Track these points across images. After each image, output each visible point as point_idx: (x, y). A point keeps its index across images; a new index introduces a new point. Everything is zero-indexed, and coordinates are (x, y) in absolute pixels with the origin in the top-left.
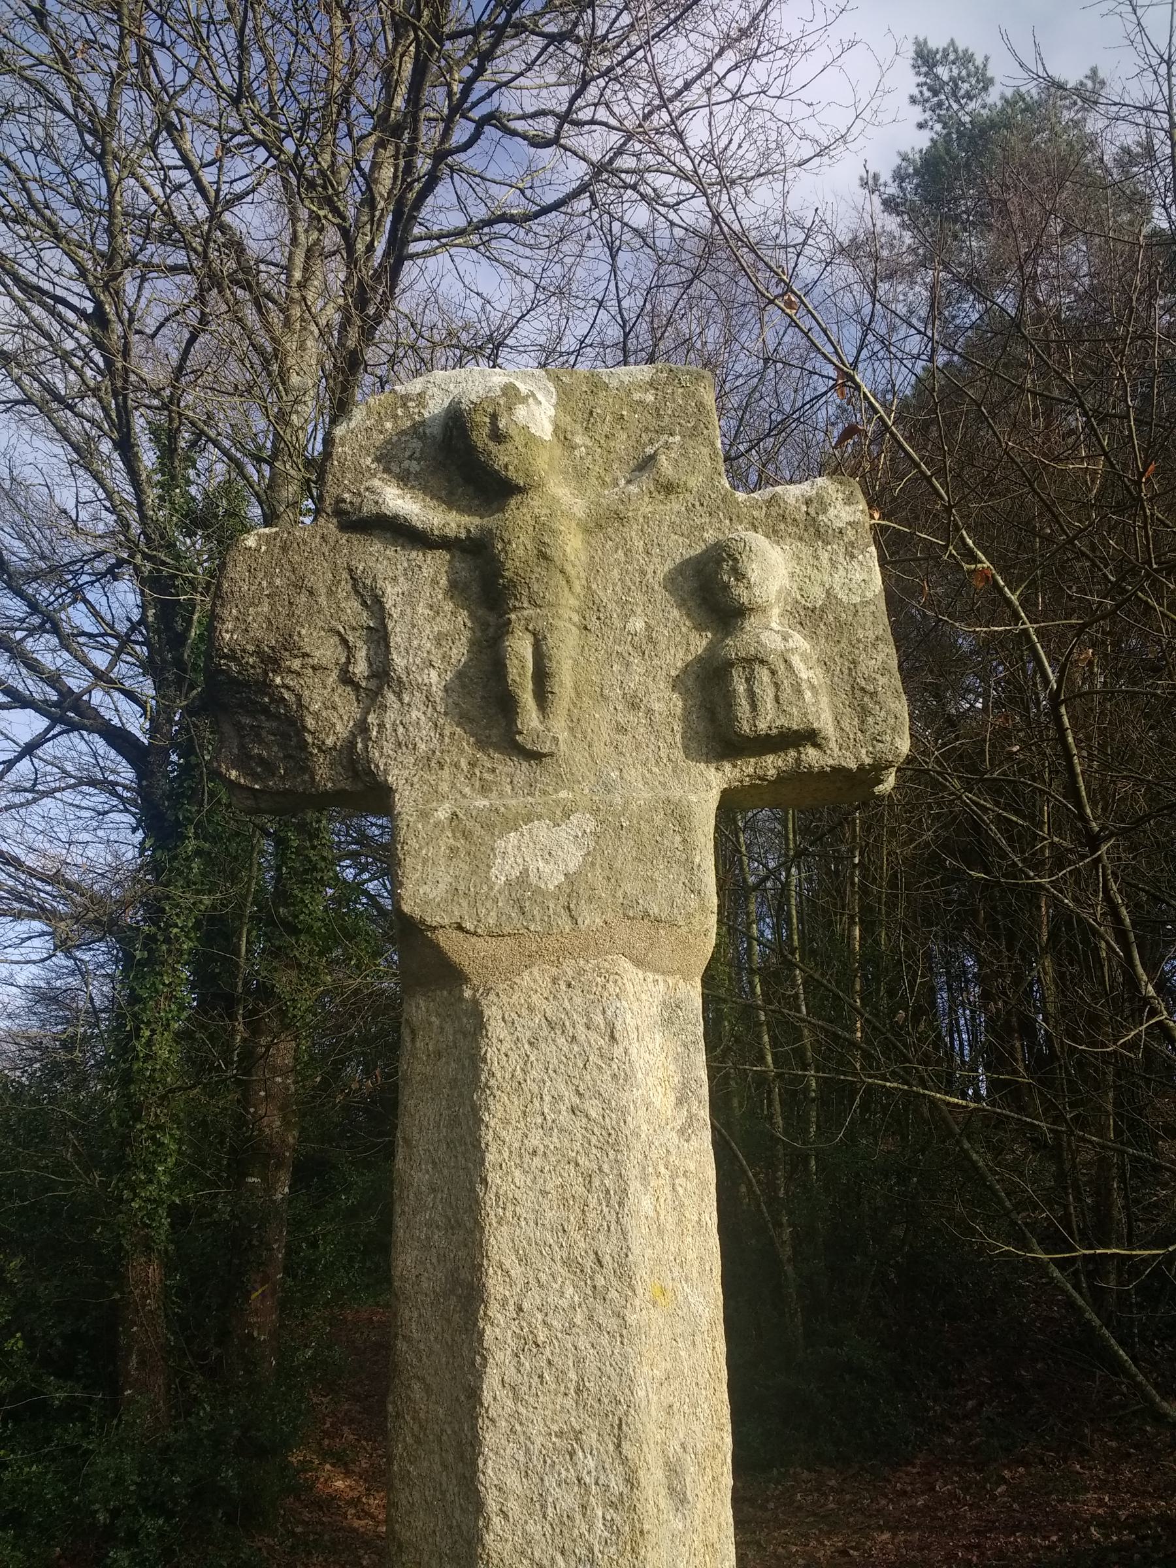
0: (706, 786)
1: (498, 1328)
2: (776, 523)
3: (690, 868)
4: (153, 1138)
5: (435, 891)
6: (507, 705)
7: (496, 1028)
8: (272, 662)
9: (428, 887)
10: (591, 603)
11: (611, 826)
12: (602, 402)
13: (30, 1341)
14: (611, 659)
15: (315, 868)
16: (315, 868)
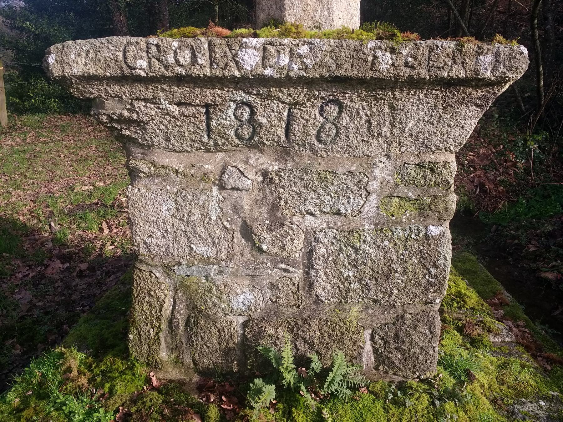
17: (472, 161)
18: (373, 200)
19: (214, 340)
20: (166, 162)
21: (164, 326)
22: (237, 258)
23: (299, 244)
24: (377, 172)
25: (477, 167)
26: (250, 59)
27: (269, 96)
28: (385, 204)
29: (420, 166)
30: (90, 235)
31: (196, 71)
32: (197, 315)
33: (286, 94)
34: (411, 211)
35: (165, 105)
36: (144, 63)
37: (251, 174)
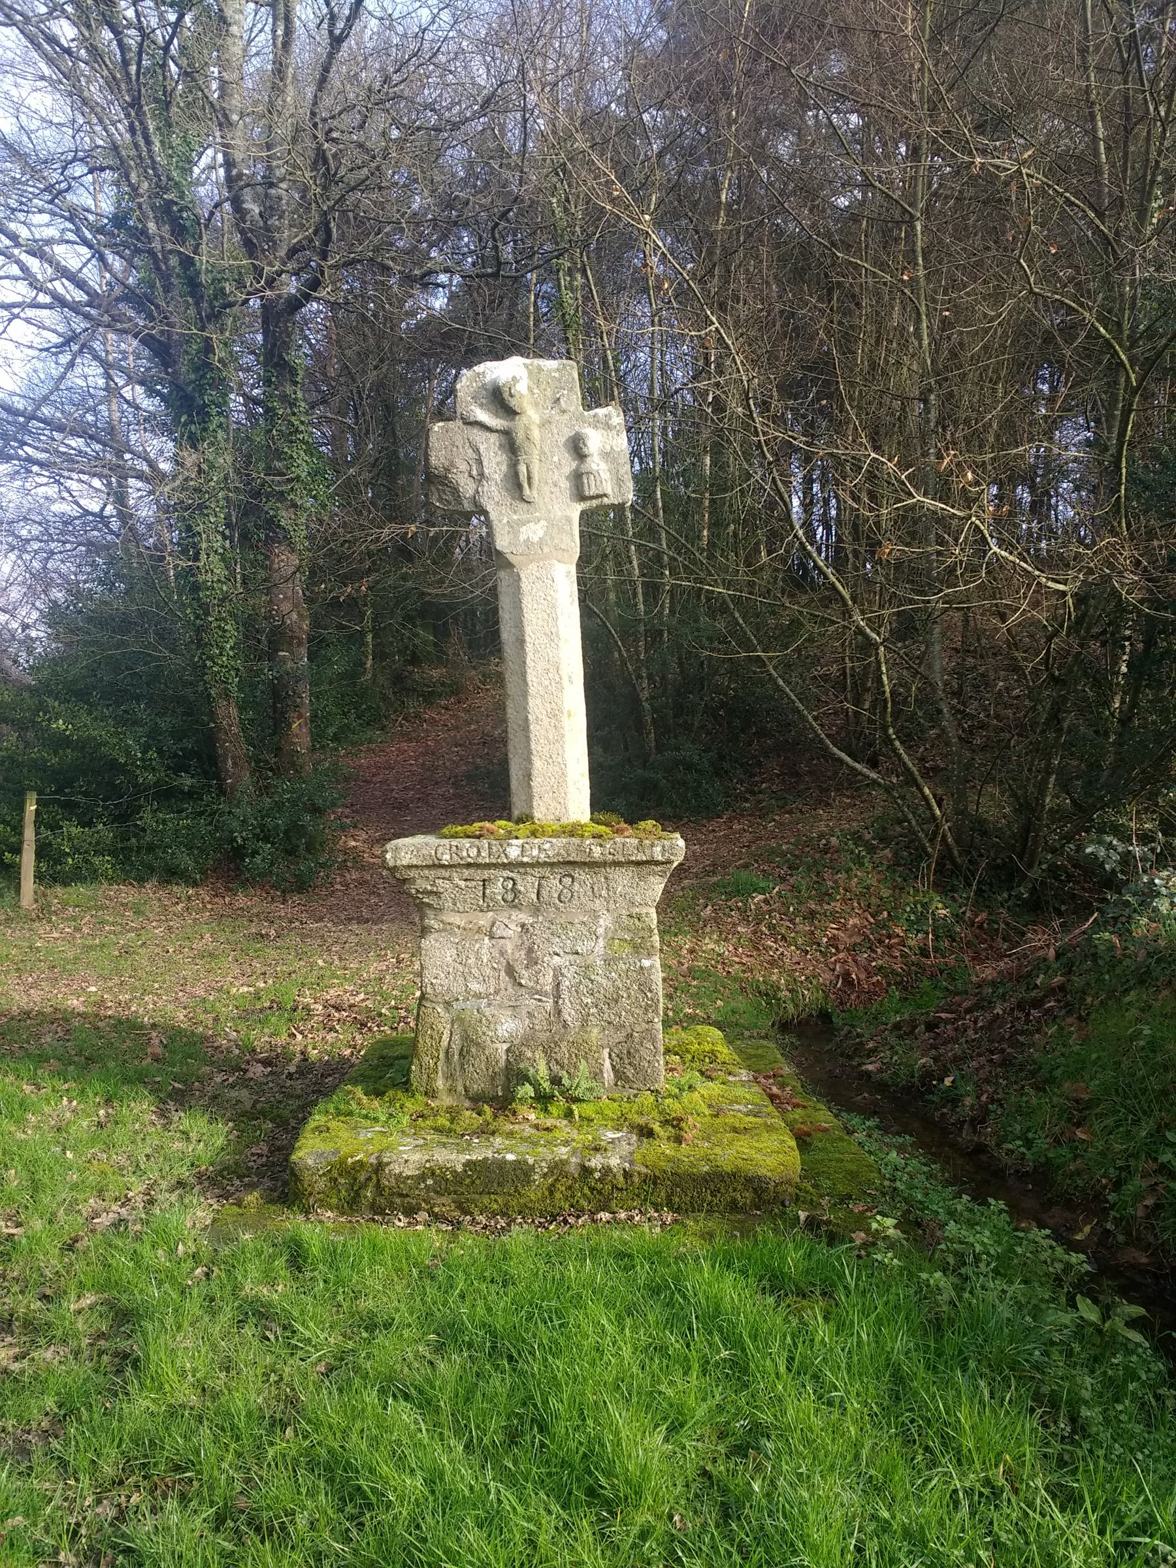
0: (575, 510)
1: (529, 648)
2: (596, 423)
3: (572, 535)
4: (219, 627)
5: (505, 544)
6: (519, 487)
7: (524, 579)
8: (448, 470)
9: (502, 542)
10: (543, 453)
11: (551, 524)
12: (542, 377)
13: (160, 751)
14: (549, 469)
15: (297, 431)
16: (297, 431)
17: (835, 937)
18: (601, 942)
19: (483, 1066)
20: (451, 920)
21: (442, 1056)
22: (503, 992)
23: (549, 978)
24: (601, 922)
25: (841, 947)
26: (514, 853)
27: (526, 873)
28: (609, 945)
29: (630, 916)
30: (282, 1039)
31: (480, 860)
32: (470, 1044)
33: (537, 872)
34: (628, 949)
35: (457, 881)
36: (447, 857)
37: (513, 926)
